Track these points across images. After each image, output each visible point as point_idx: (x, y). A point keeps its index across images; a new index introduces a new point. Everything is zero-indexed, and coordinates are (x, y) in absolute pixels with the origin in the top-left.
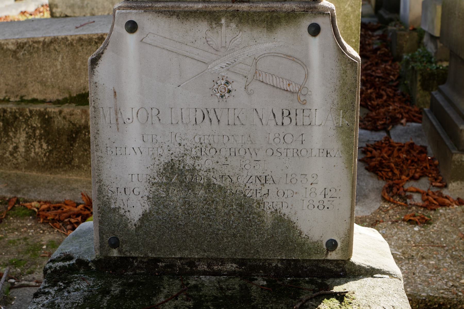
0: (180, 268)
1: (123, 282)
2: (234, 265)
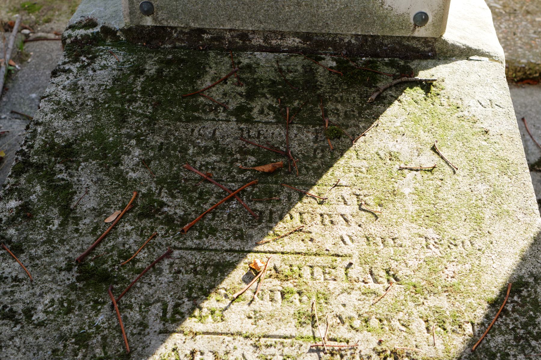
0: (229, 42)
1: (160, 58)
2: (298, 40)
